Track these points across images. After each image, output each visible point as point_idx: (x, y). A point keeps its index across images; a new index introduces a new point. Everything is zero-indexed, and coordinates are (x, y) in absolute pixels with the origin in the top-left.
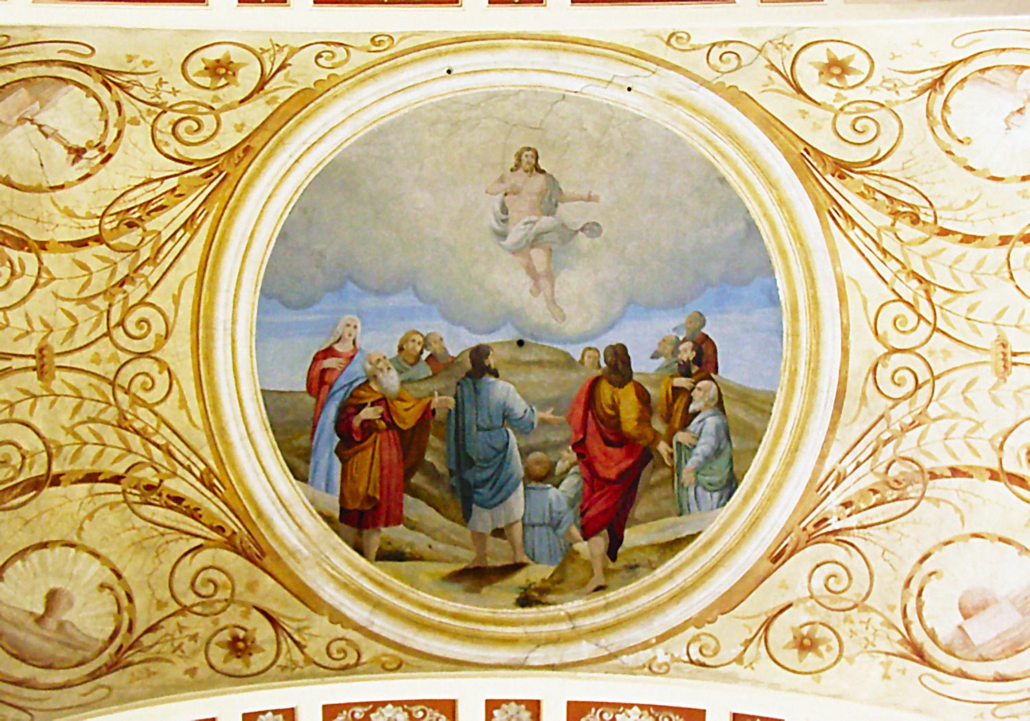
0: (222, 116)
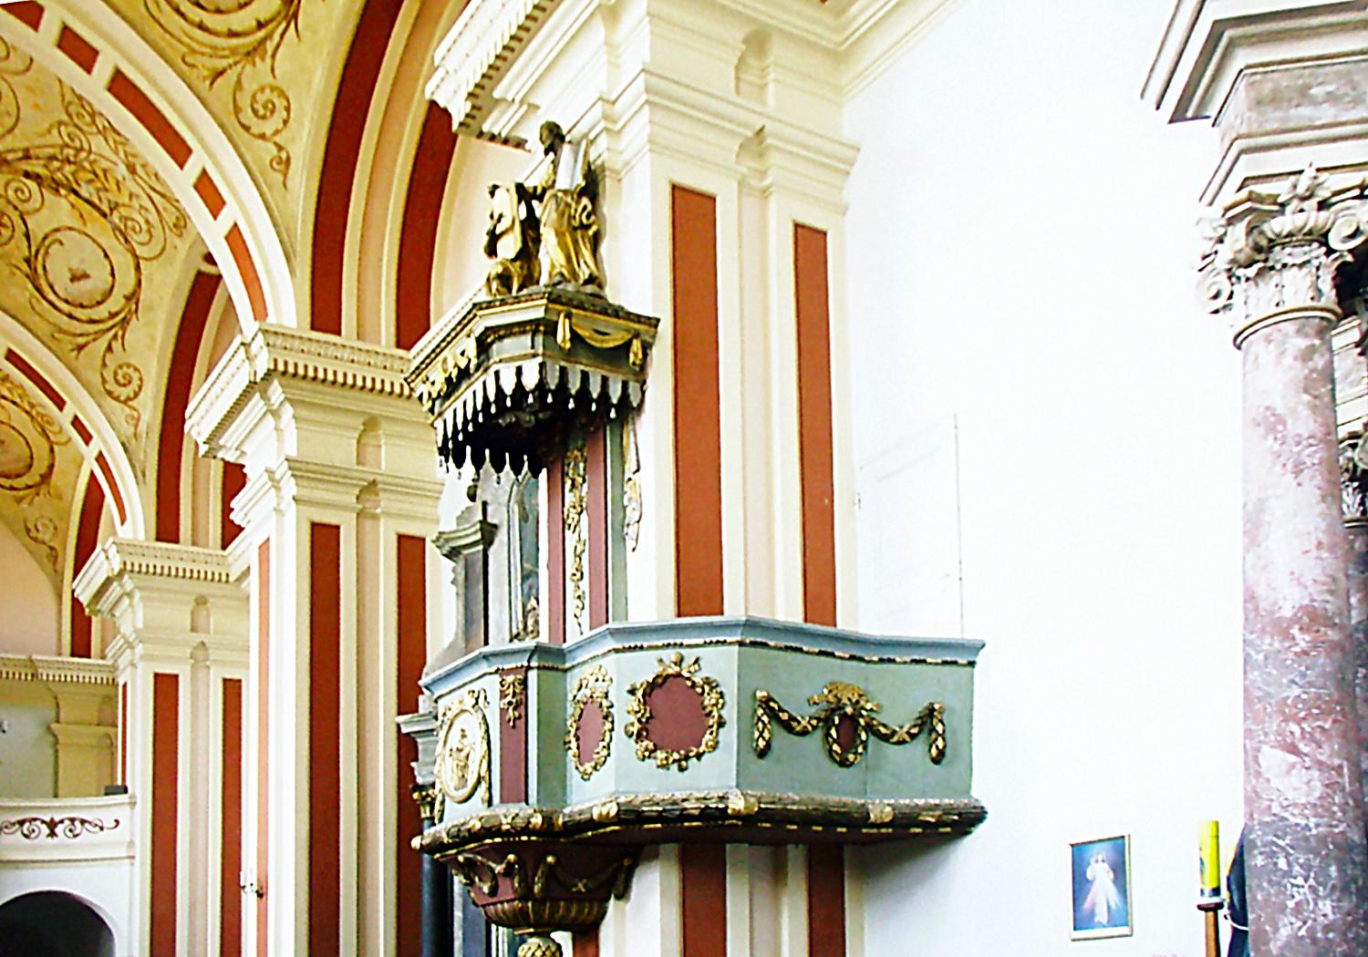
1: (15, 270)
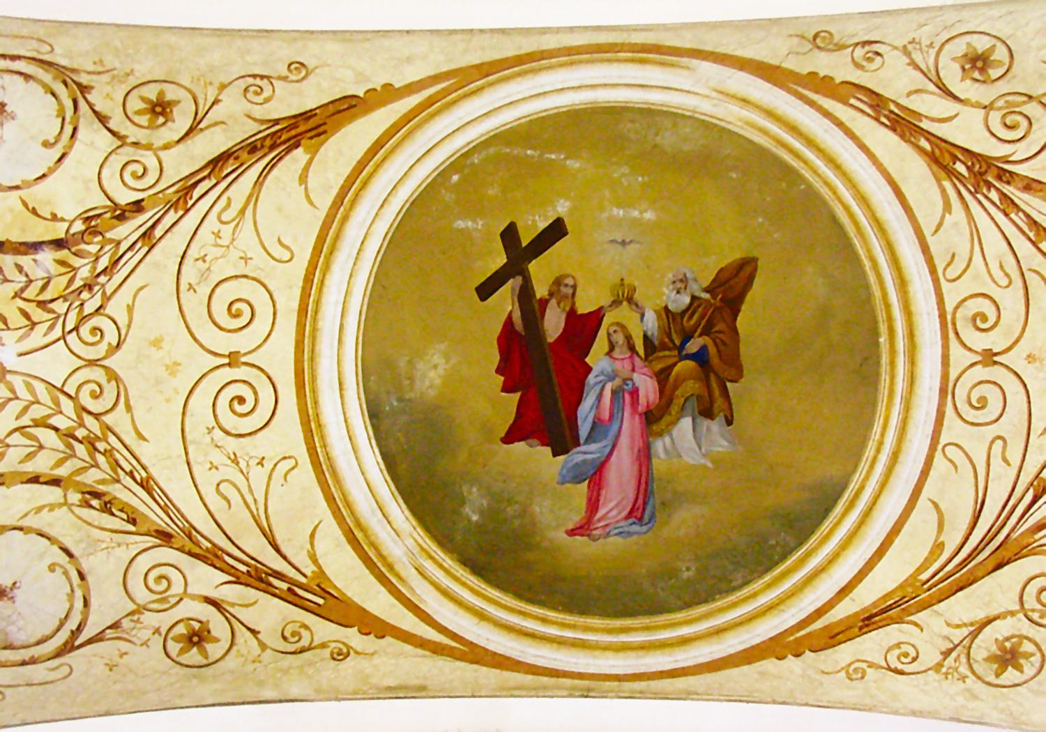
0: (1017, 607)
1: (100, 69)
